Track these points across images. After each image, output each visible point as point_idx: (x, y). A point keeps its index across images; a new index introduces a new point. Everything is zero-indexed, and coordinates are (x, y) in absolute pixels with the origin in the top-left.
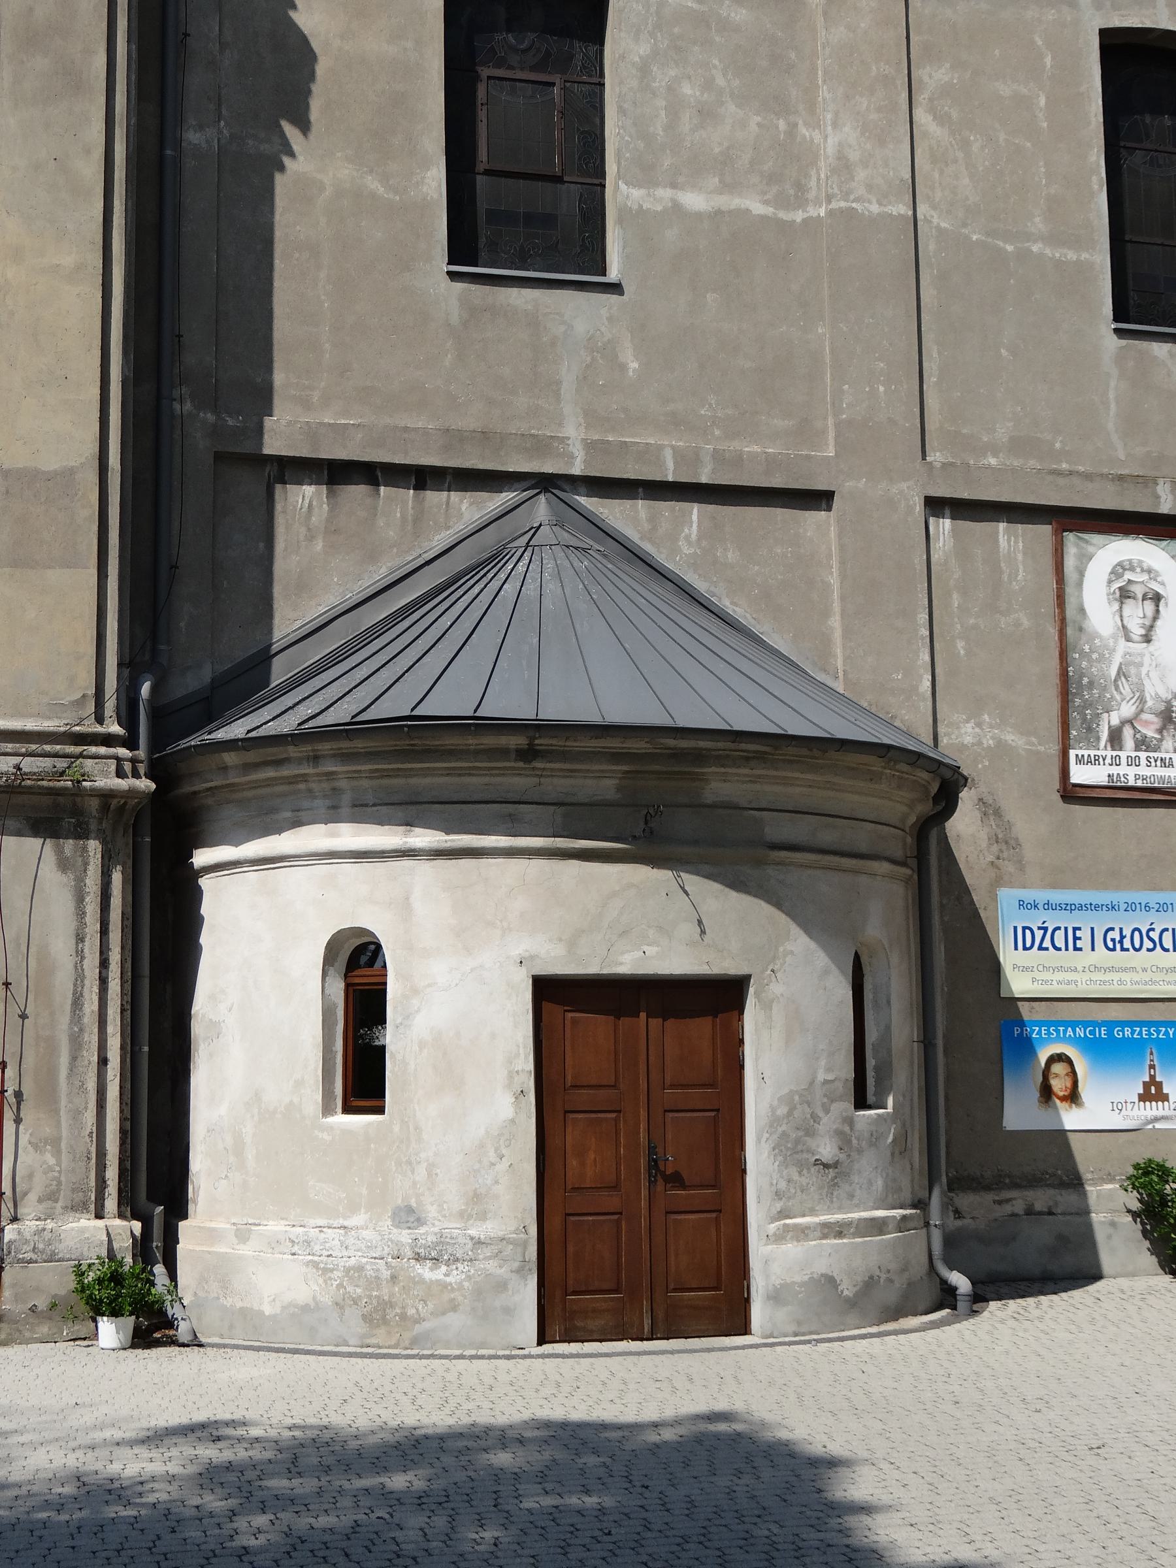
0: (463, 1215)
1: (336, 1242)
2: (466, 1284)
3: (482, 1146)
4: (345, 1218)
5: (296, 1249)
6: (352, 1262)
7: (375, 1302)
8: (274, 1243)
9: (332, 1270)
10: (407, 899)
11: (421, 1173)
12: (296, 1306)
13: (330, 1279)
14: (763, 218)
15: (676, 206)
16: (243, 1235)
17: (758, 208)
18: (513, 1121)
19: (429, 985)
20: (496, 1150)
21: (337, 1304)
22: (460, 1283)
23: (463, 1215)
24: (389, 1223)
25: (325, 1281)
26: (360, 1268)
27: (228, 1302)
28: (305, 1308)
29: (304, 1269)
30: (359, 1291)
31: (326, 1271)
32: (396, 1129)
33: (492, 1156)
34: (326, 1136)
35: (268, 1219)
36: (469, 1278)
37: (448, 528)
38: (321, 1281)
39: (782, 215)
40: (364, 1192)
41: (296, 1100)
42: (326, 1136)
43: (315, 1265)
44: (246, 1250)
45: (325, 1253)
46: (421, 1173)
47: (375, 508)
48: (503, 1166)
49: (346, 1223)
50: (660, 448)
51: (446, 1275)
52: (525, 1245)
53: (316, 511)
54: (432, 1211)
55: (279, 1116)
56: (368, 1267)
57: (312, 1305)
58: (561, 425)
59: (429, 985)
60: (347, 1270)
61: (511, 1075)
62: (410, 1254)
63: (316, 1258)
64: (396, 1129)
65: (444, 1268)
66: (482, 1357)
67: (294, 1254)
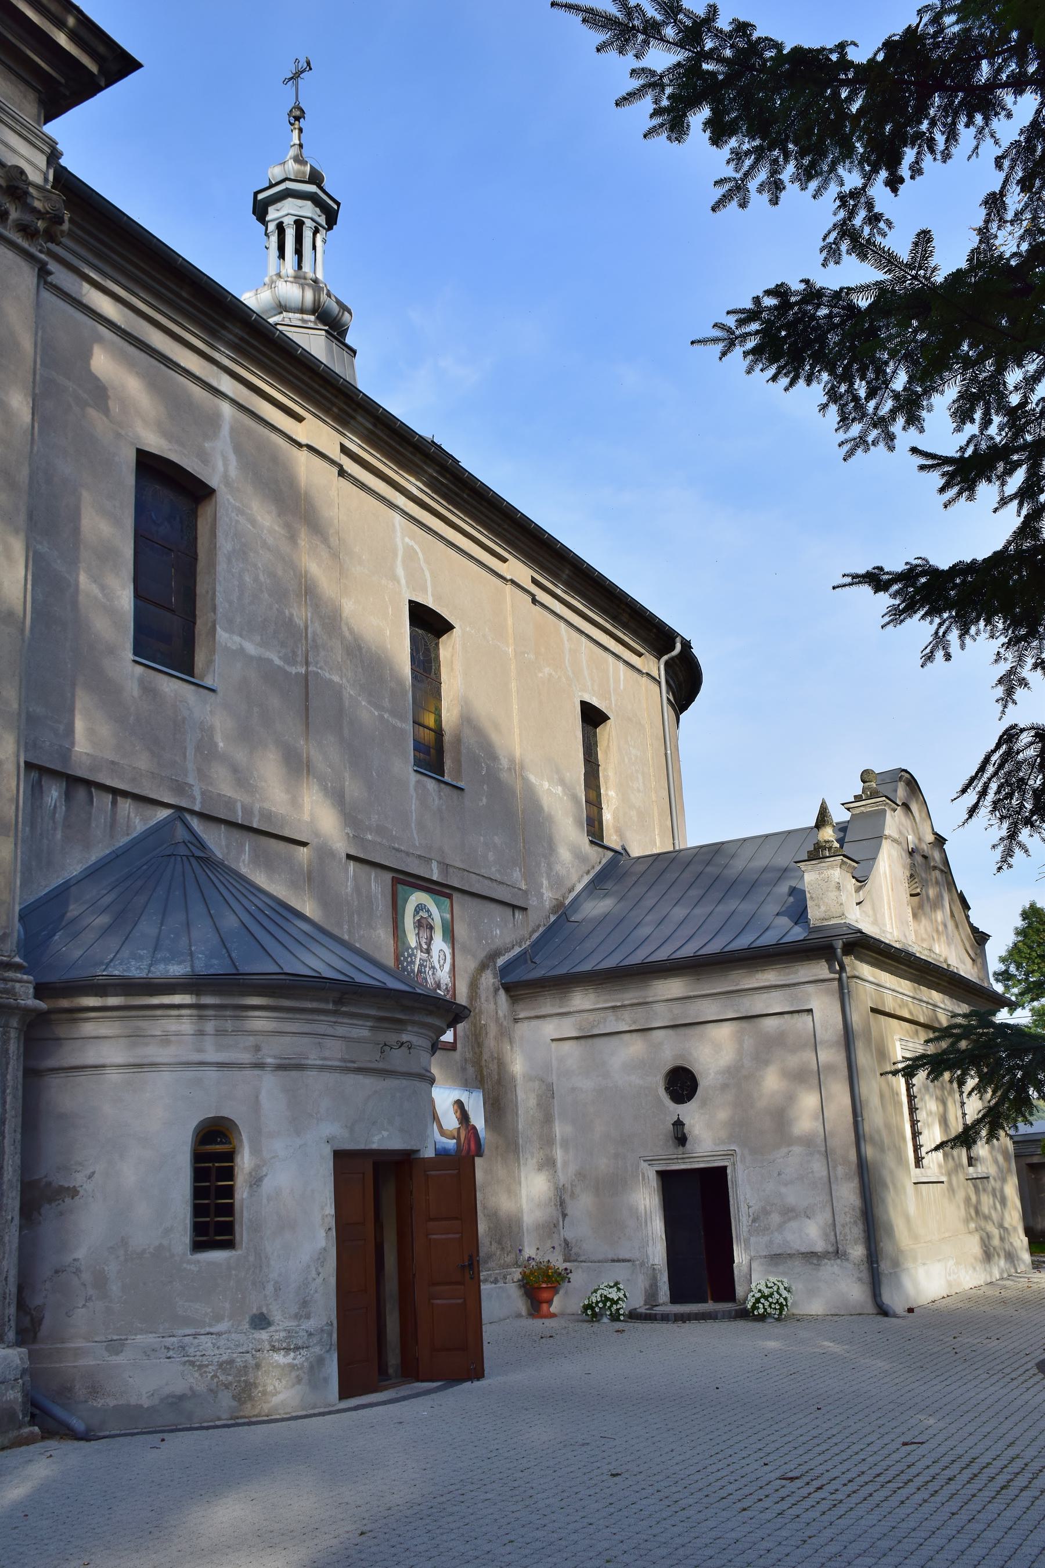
0: (297, 1317)
1: (209, 1344)
2: (305, 1364)
3: (309, 1266)
4: (211, 1326)
5: (171, 1353)
6: (225, 1358)
7: (243, 1385)
8: (149, 1352)
9: (207, 1366)
10: (257, 1097)
11: (270, 1288)
12: (174, 1396)
13: (205, 1372)
14: (279, 667)
15: (242, 650)
16: (115, 1347)
17: (278, 662)
18: (325, 1249)
19: (273, 1157)
20: (317, 1269)
21: (211, 1390)
22: (302, 1364)
23: (297, 1317)
24: (247, 1326)
25: (201, 1375)
26: (231, 1362)
27: (99, 1403)
28: (182, 1398)
29: (181, 1368)
30: (230, 1378)
31: (200, 1367)
32: (251, 1259)
33: (314, 1274)
34: (193, 1267)
35: (136, 1334)
36: (307, 1359)
37: (128, 835)
38: (197, 1375)
39: (287, 668)
40: (227, 1305)
41: (165, 1242)
42: (193, 1267)
43: (192, 1363)
44: (120, 1359)
45: (198, 1353)
46: (270, 1288)
47: (90, 814)
48: (319, 1280)
49: (212, 1330)
50: (236, 801)
51: (294, 1359)
52: (330, 1335)
53: (58, 810)
54: (276, 1316)
55: (147, 1255)
56: (238, 1360)
57: (189, 1393)
58: (186, 775)
59: (273, 1157)
60: (220, 1365)
61: (324, 1217)
62: (268, 1347)
63: (191, 1359)
64: (251, 1259)
65: (292, 1354)
66: (217, 1427)
67: (169, 1358)
